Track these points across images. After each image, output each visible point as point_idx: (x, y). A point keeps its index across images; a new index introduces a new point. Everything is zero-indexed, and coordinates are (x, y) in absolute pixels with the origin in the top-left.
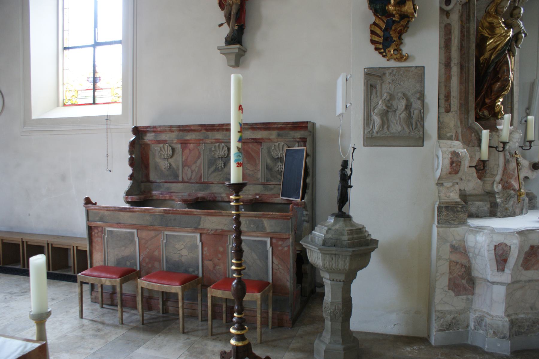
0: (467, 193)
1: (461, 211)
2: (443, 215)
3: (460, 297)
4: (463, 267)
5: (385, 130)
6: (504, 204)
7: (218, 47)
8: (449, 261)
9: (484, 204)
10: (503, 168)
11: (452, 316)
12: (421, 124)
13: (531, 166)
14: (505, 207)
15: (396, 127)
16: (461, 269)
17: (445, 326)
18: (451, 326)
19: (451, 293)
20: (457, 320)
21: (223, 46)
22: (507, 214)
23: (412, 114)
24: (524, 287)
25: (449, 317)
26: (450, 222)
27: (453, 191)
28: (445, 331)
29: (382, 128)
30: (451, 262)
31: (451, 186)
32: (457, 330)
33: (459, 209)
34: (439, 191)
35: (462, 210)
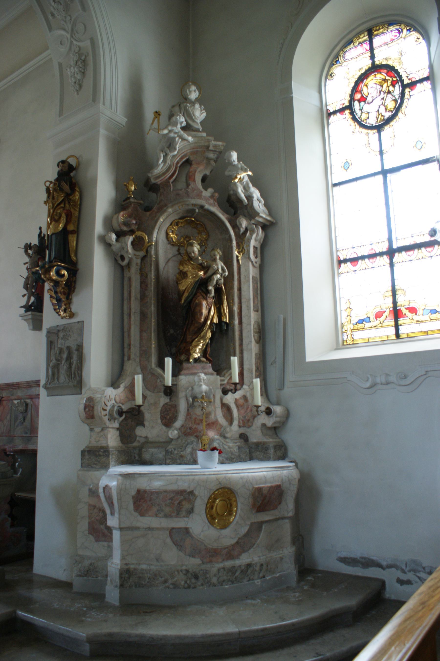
0: (150, 440)
1: (103, 456)
2: (85, 459)
3: (101, 543)
4: (101, 511)
5: (56, 381)
6: (178, 451)
7: (20, 315)
8: (88, 504)
9: (159, 451)
10: (186, 413)
11: (90, 562)
12: (78, 374)
13: (272, 414)
14: (180, 454)
15: (63, 377)
16: (99, 513)
17: (82, 572)
18: (89, 572)
19: (91, 538)
20: (95, 566)
21: (24, 314)
22: (183, 462)
23: (72, 365)
24: (146, 535)
25: (87, 563)
26: (92, 465)
27: (102, 435)
28: (83, 577)
29: (53, 379)
30: (90, 505)
31: (100, 432)
32: (96, 577)
33: (101, 453)
34: (91, 436)
35: (105, 455)
